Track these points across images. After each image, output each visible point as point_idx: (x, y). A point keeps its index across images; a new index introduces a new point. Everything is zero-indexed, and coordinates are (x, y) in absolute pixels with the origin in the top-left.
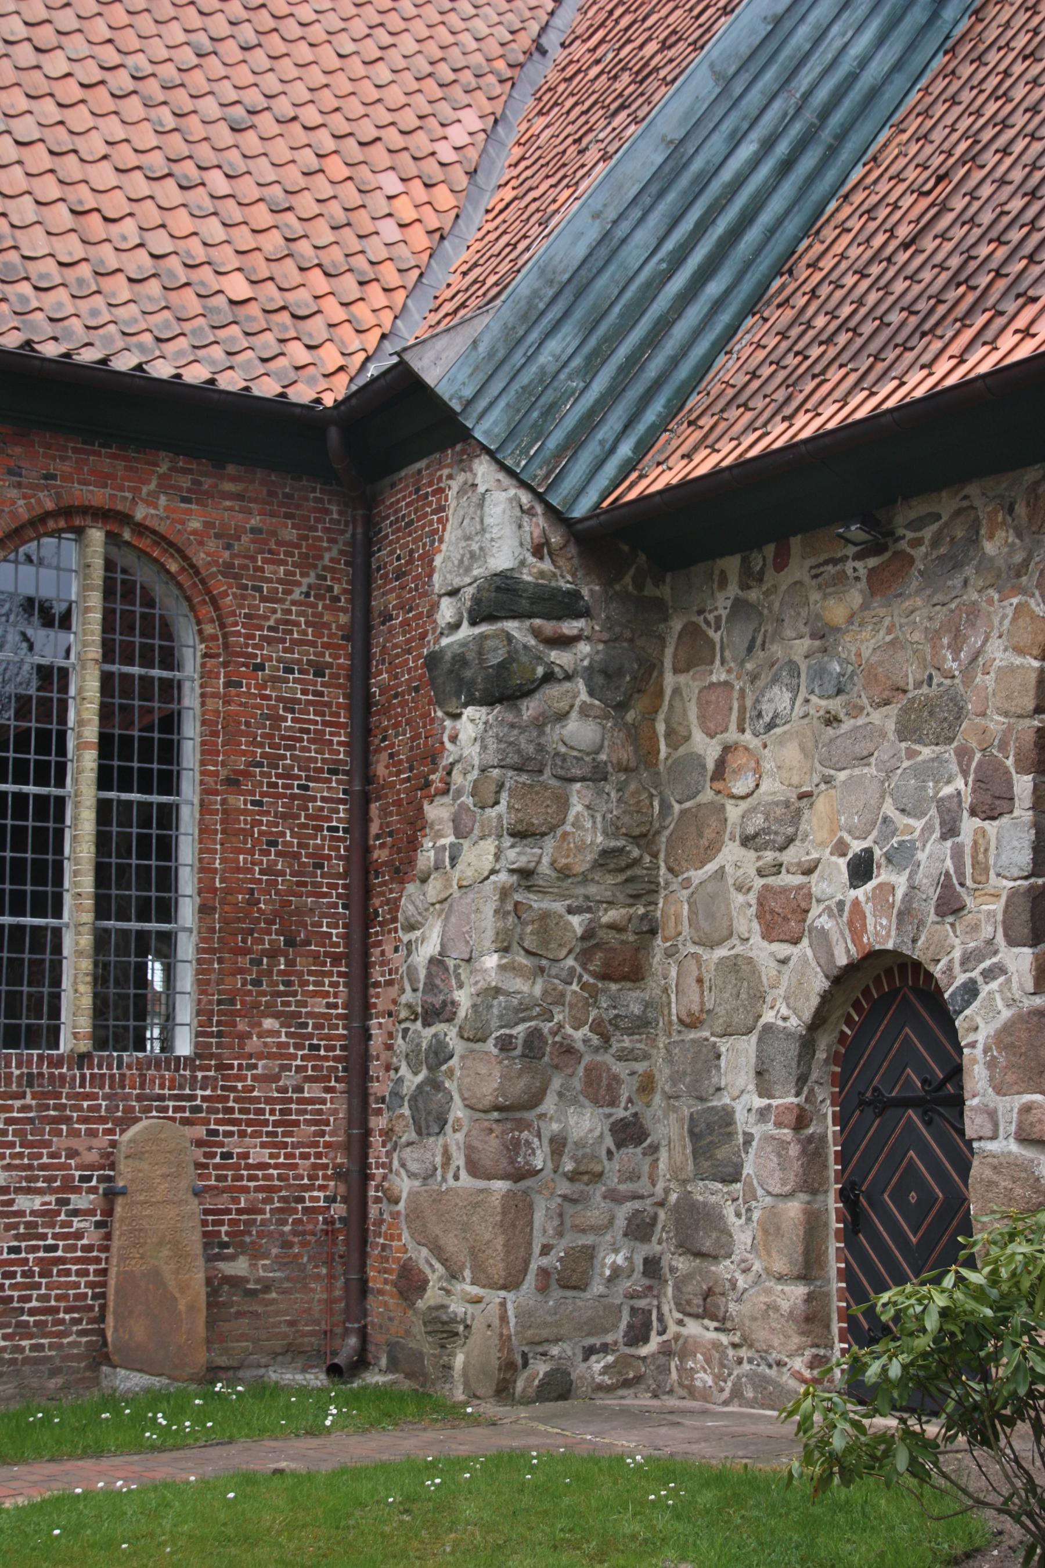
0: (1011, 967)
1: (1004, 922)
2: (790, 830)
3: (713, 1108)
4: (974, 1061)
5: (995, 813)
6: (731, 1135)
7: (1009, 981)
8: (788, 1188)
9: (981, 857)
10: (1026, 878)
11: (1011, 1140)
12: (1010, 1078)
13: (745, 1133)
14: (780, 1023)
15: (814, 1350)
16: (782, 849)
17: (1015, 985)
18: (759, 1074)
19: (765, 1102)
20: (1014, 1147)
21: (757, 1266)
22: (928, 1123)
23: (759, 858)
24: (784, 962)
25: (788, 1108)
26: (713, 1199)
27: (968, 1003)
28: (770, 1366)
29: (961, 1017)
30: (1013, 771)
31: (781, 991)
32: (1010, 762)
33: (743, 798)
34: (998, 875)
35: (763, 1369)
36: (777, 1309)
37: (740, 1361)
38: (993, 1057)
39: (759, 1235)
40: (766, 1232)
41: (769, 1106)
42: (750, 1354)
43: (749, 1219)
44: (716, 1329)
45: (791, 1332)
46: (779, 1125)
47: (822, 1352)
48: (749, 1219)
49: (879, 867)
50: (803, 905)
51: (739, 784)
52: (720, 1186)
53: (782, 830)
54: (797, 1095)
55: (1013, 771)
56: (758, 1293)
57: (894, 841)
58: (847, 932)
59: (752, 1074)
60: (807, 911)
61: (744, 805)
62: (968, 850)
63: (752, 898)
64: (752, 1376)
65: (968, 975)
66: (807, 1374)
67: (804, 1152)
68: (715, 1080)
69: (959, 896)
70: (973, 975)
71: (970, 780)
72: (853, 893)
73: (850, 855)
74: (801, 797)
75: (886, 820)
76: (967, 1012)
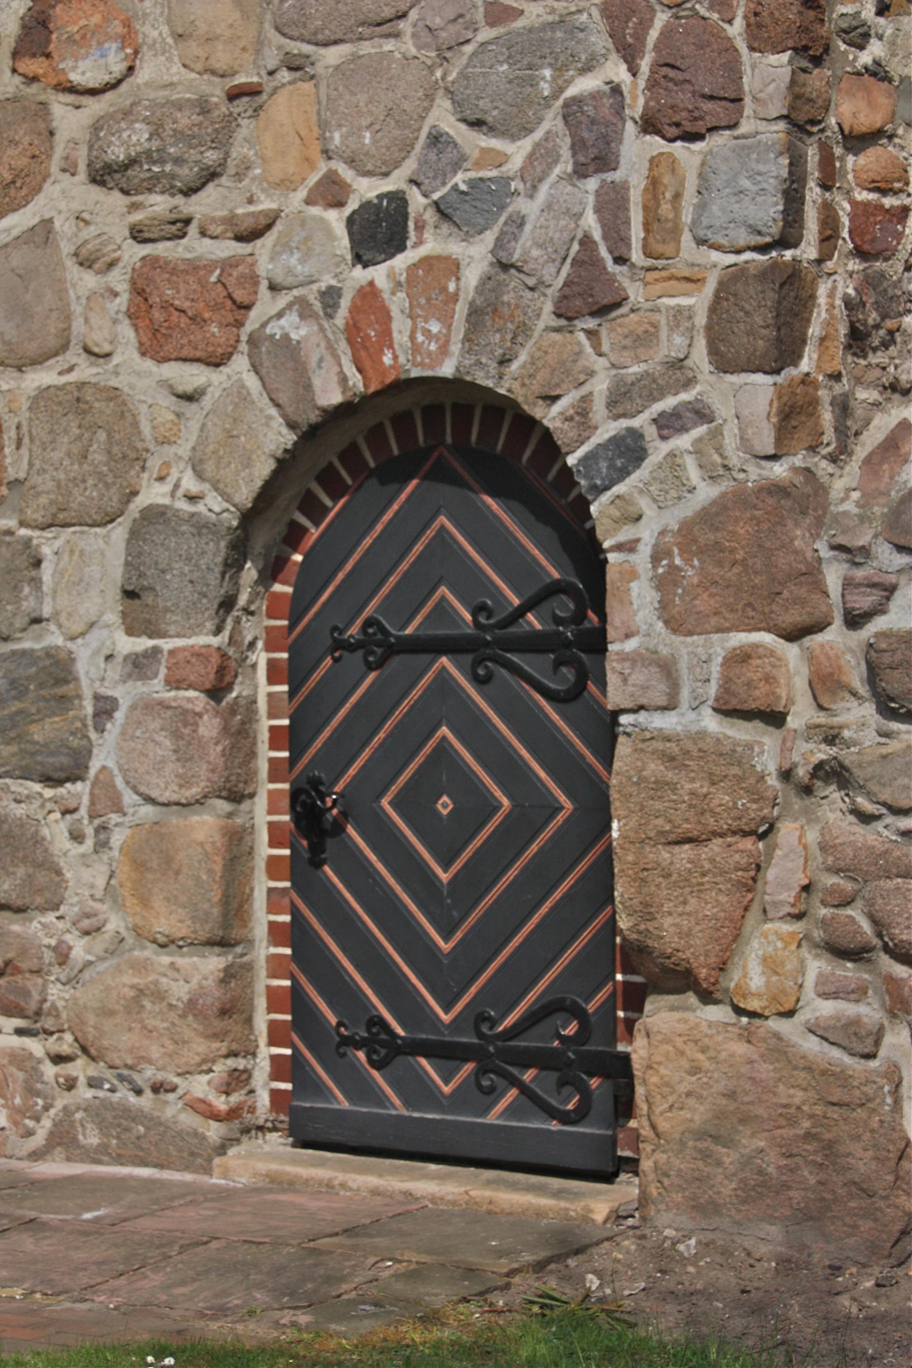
0: (723, 410)
1: (709, 328)
2: (211, 157)
3: (24, 653)
4: (633, 575)
5: (700, 127)
6: (64, 702)
7: (717, 433)
8: (194, 791)
9: (665, 209)
10: (762, 249)
11: (707, 711)
12: (704, 603)
13: (97, 697)
14: (183, 505)
15: (231, 1063)
16: (189, 191)
17: (730, 441)
18: (130, 594)
19: (144, 643)
20: (711, 723)
21: (115, 923)
22: (480, 682)
23: (134, 207)
24: (190, 398)
25: (200, 654)
26: (19, 811)
27: (623, 474)
28: (139, 1092)
29: (606, 497)
30: (742, 46)
31: (184, 449)
32: (736, 29)
33: (93, 92)
34: (701, 242)
35: (124, 1095)
36: (159, 995)
37: (70, 1085)
38: (672, 567)
39: (124, 872)
40: (139, 865)
41: (156, 650)
42: (93, 1070)
43: (102, 845)
44: (20, 1032)
45: (188, 1033)
46: (174, 683)
47: (241, 1063)
48: (102, 845)
49: (420, 227)
50: (240, 295)
51: (83, 65)
52: (37, 787)
53: (193, 154)
54: (218, 630)
55: (742, 46)
56: (118, 970)
57: (460, 179)
58: (343, 347)
59: (114, 594)
60: (248, 307)
61: (96, 107)
62: (636, 197)
63: (119, 280)
64: (95, 1111)
65: (624, 423)
66: (221, 1103)
67: (225, 729)
68: (28, 605)
69: (612, 279)
70: (634, 423)
71: (645, 65)
72: (360, 275)
73: (353, 205)
74: (234, 95)
75: (436, 139)
76: (619, 489)
